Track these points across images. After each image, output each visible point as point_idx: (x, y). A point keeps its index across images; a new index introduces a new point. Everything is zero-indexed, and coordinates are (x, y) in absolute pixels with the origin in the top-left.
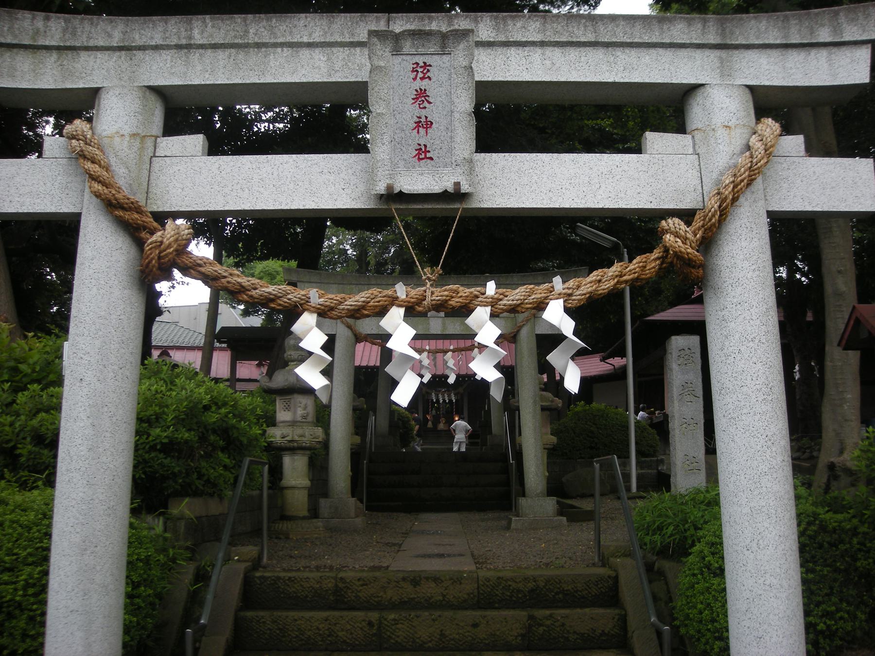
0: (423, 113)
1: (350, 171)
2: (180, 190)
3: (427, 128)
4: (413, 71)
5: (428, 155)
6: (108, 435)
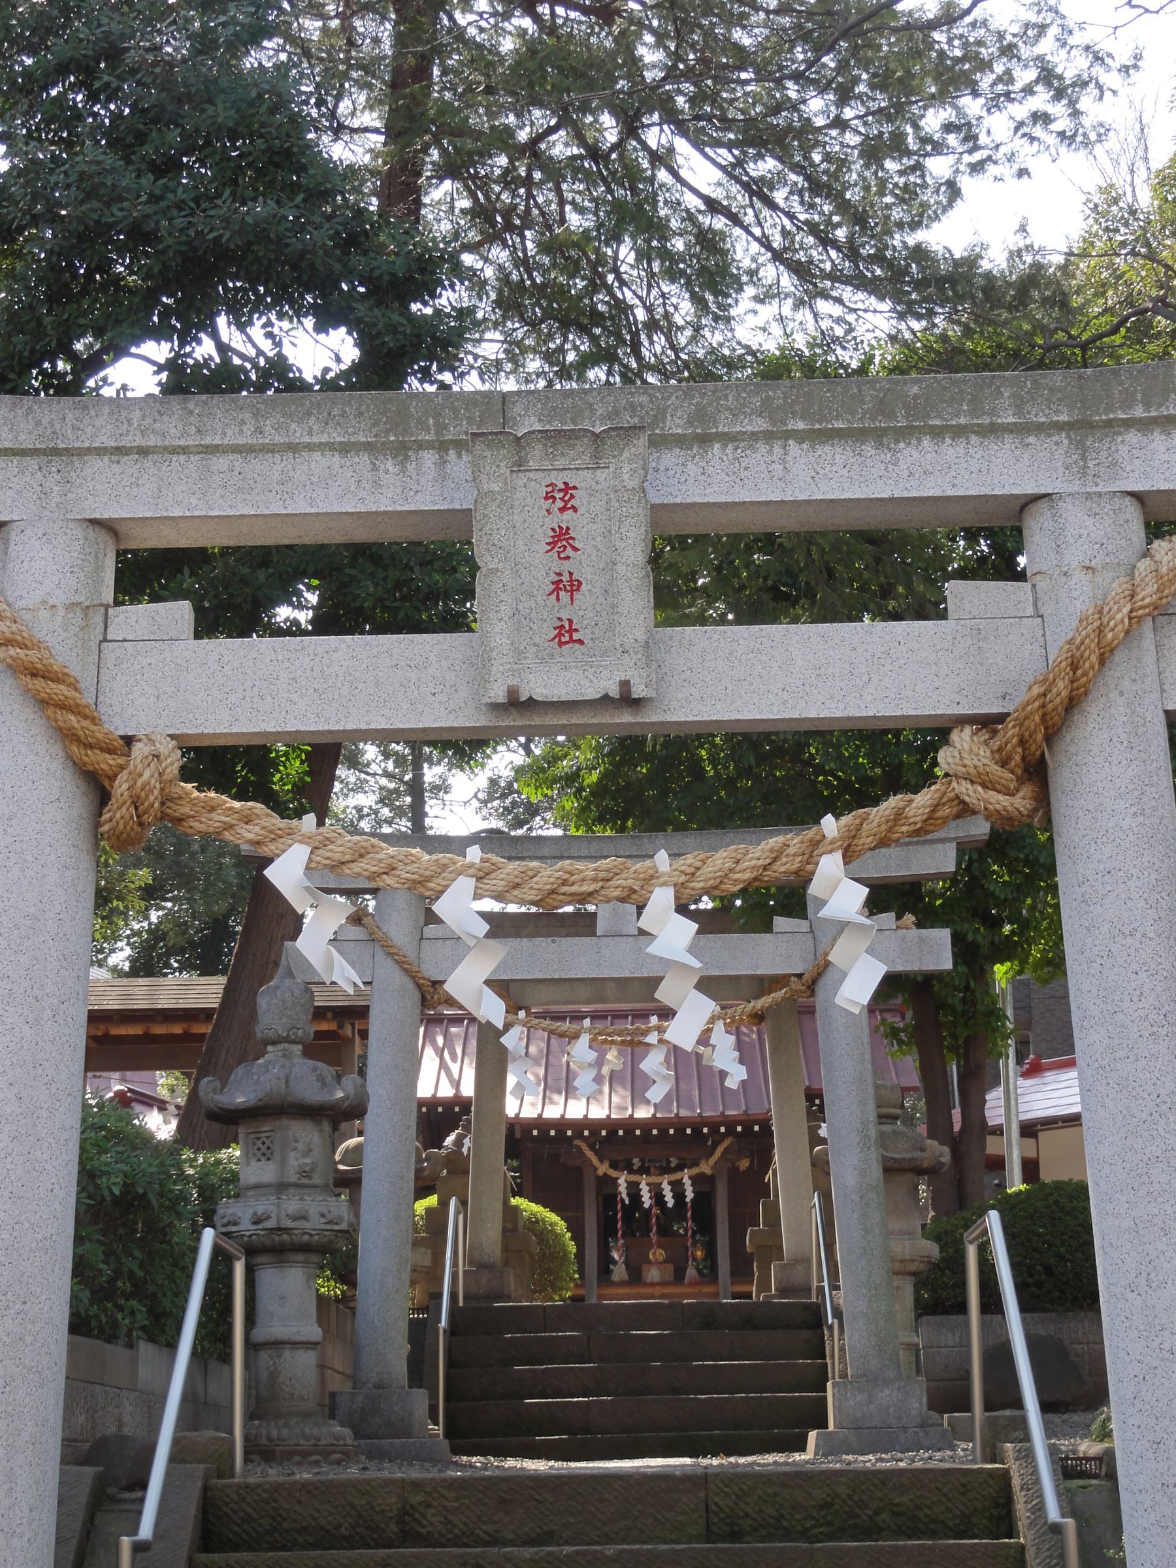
0: (566, 566)
1: (444, 663)
2: (153, 699)
3: (572, 592)
4: (546, 498)
5: (576, 636)
6: (44, 1113)
